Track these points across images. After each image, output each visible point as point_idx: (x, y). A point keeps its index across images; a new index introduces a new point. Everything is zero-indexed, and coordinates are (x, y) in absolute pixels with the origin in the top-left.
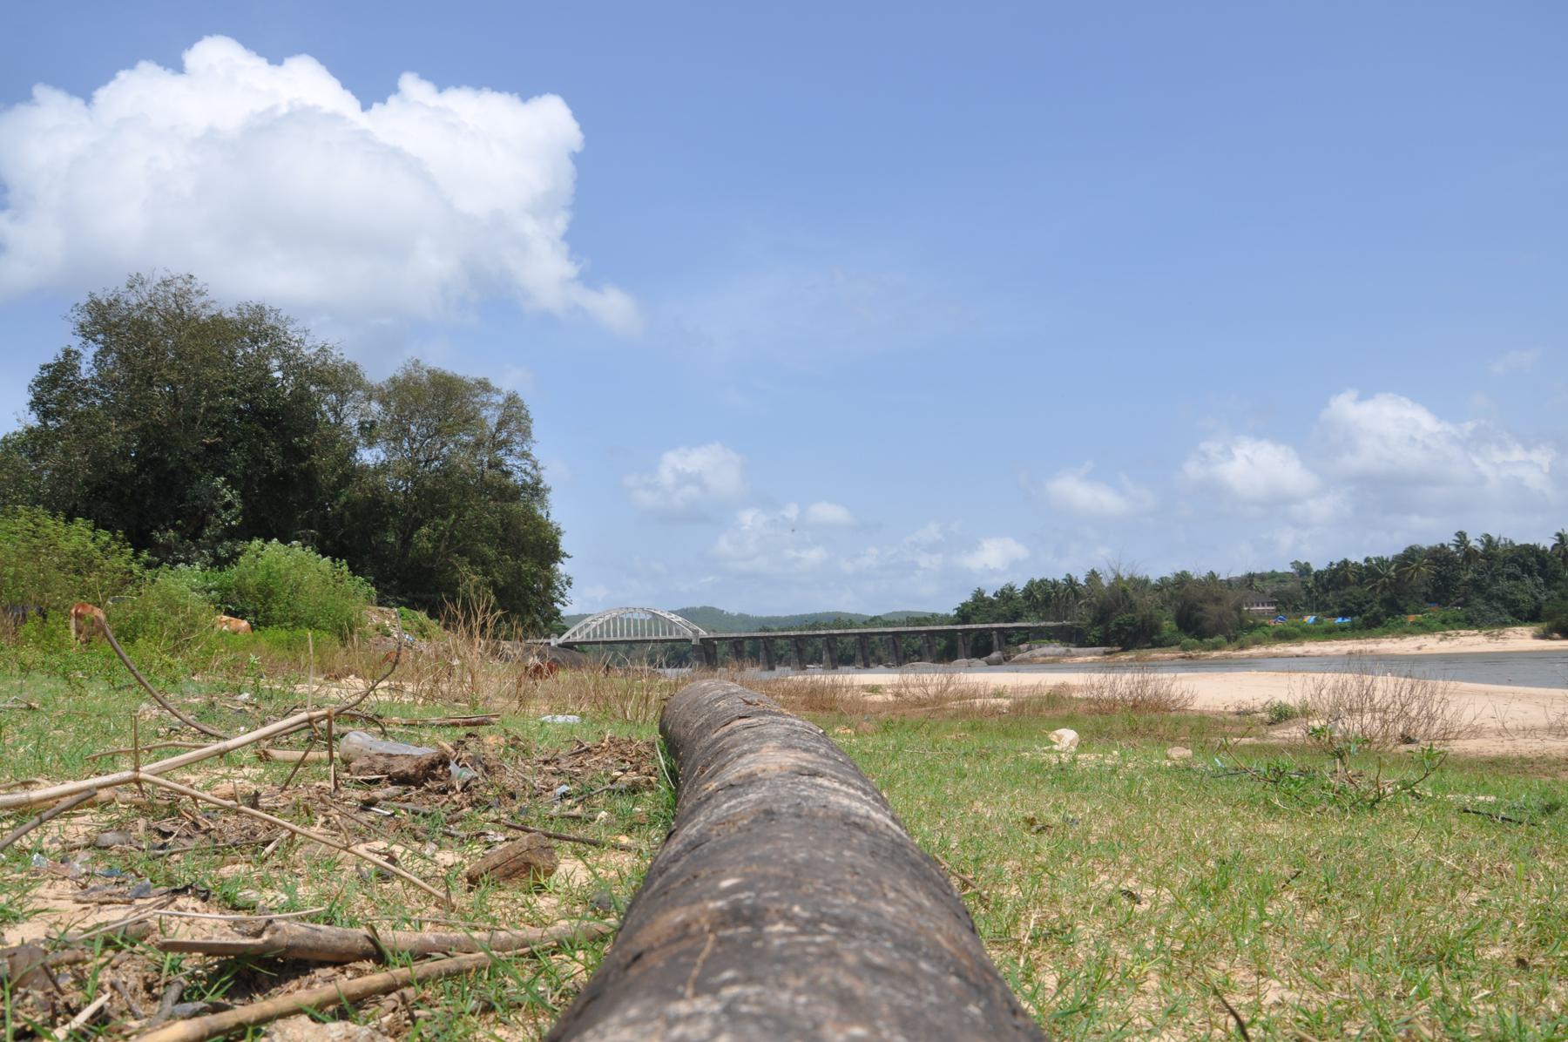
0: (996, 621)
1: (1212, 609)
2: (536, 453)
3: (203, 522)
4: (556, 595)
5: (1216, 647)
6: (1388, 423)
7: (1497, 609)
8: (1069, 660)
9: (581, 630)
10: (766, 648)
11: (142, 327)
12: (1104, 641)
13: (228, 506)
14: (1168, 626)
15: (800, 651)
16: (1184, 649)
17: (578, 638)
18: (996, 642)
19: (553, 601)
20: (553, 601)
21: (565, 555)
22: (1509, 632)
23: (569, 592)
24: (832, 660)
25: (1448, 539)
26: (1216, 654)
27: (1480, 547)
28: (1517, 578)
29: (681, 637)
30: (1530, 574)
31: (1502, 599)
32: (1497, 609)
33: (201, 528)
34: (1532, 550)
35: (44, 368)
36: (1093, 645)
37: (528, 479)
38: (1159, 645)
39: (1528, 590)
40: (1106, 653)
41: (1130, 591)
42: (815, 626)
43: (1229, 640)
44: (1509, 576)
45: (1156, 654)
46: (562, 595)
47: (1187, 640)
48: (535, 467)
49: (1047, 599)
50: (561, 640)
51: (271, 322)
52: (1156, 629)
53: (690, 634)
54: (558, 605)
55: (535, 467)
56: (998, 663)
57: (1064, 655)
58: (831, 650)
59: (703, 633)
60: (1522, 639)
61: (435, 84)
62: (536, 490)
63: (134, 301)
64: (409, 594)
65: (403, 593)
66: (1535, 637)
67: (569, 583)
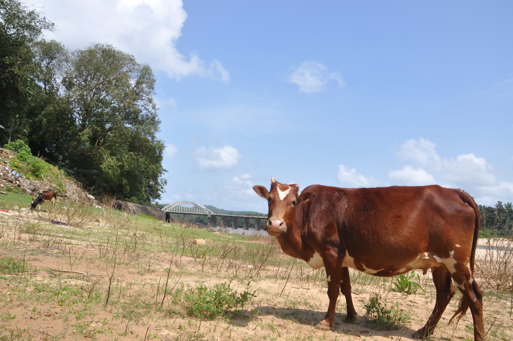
2: (155, 101)
4: (160, 188)
9: (168, 208)
10: (235, 221)
19: (158, 190)
20: (158, 190)
21: (165, 170)
23: (165, 187)
24: (258, 227)
29: (204, 214)
34: (490, 208)
37: (150, 116)
46: (162, 188)
48: (154, 108)
53: (208, 213)
54: (160, 192)
55: (154, 108)
58: (258, 224)
59: (212, 213)
61: (180, 38)
62: (152, 122)
64: (75, 169)
65: (71, 168)
67: (166, 183)
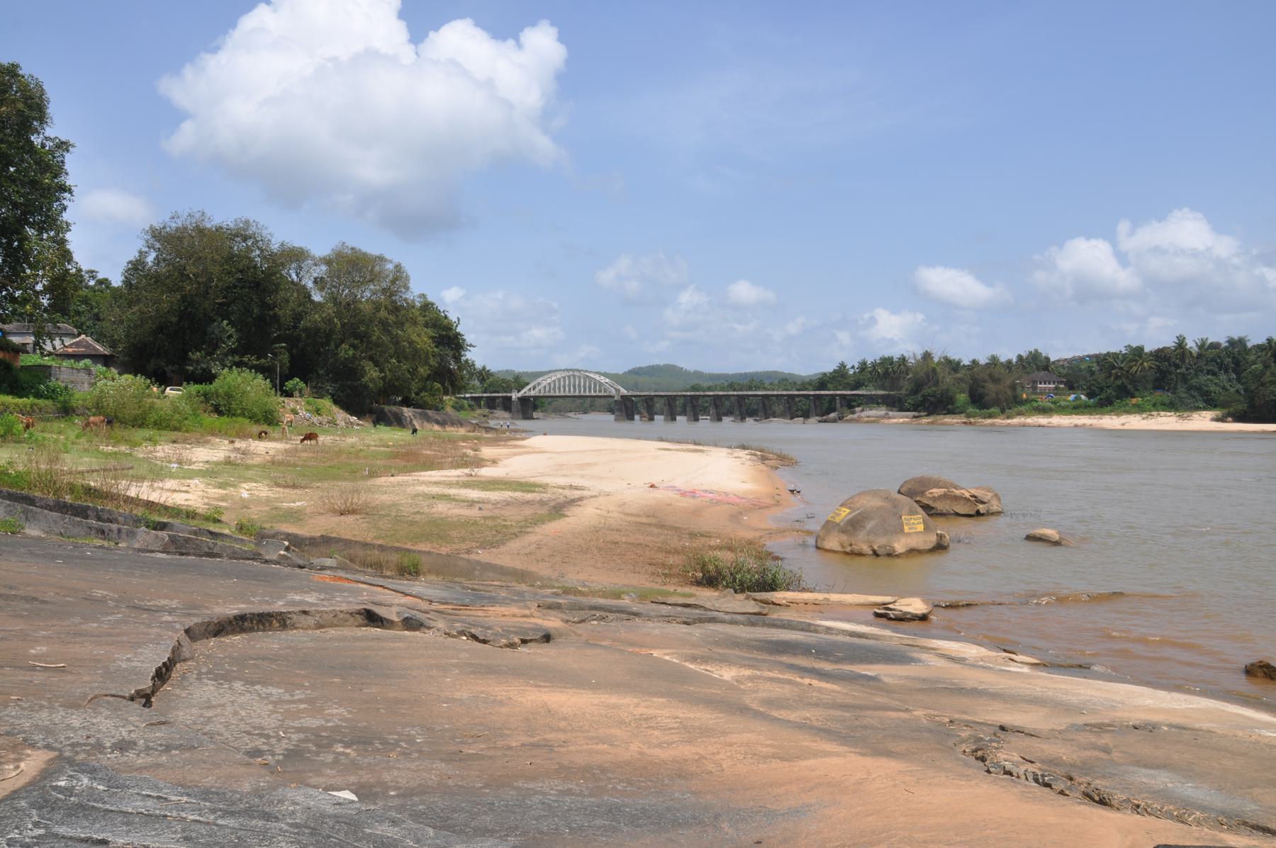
0: (844, 389)
1: (991, 387)
3: (216, 347)
5: (990, 416)
6: (1188, 235)
7: (1194, 397)
8: (886, 421)
11: (180, 239)
12: (915, 408)
13: (230, 337)
14: (962, 398)
15: (694, 407)
16: (968, 416)
17: (533, 393)
18: (838, 405)
22: (1195, 415)
24: (741, 414)
25: (1168, 342)
26: (989, 421)
27: (1195, 350)
28: (1214, 374)
30: (1226, 371)
31: (1199, 389)
32: (1194, 397)
33: (215, 350)
35: (130, 262)
36: (908, 410)
38: (951, 412)
39: (1222, 383)
40: (914, 417)
41: (939, 370)
42: (731, 387)
43: (1003, 411)
44: (1208, 372)
45: (948, 419)
47: (971, 410)
49: (886, 374)
50: (520, 395)
51: (254, 229)
52: (951, 400)
56: (834, 421)
57: (884, 417)
58: (716, 406)
59: (624, 392)
60: (1203, 421)
63: (174, 225)
66: (1213, 420)
